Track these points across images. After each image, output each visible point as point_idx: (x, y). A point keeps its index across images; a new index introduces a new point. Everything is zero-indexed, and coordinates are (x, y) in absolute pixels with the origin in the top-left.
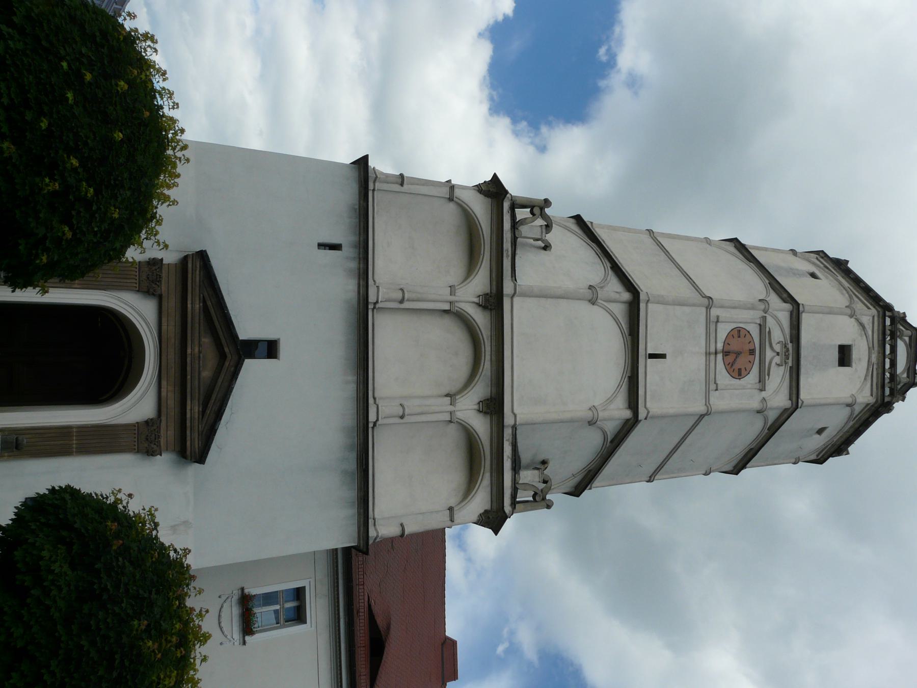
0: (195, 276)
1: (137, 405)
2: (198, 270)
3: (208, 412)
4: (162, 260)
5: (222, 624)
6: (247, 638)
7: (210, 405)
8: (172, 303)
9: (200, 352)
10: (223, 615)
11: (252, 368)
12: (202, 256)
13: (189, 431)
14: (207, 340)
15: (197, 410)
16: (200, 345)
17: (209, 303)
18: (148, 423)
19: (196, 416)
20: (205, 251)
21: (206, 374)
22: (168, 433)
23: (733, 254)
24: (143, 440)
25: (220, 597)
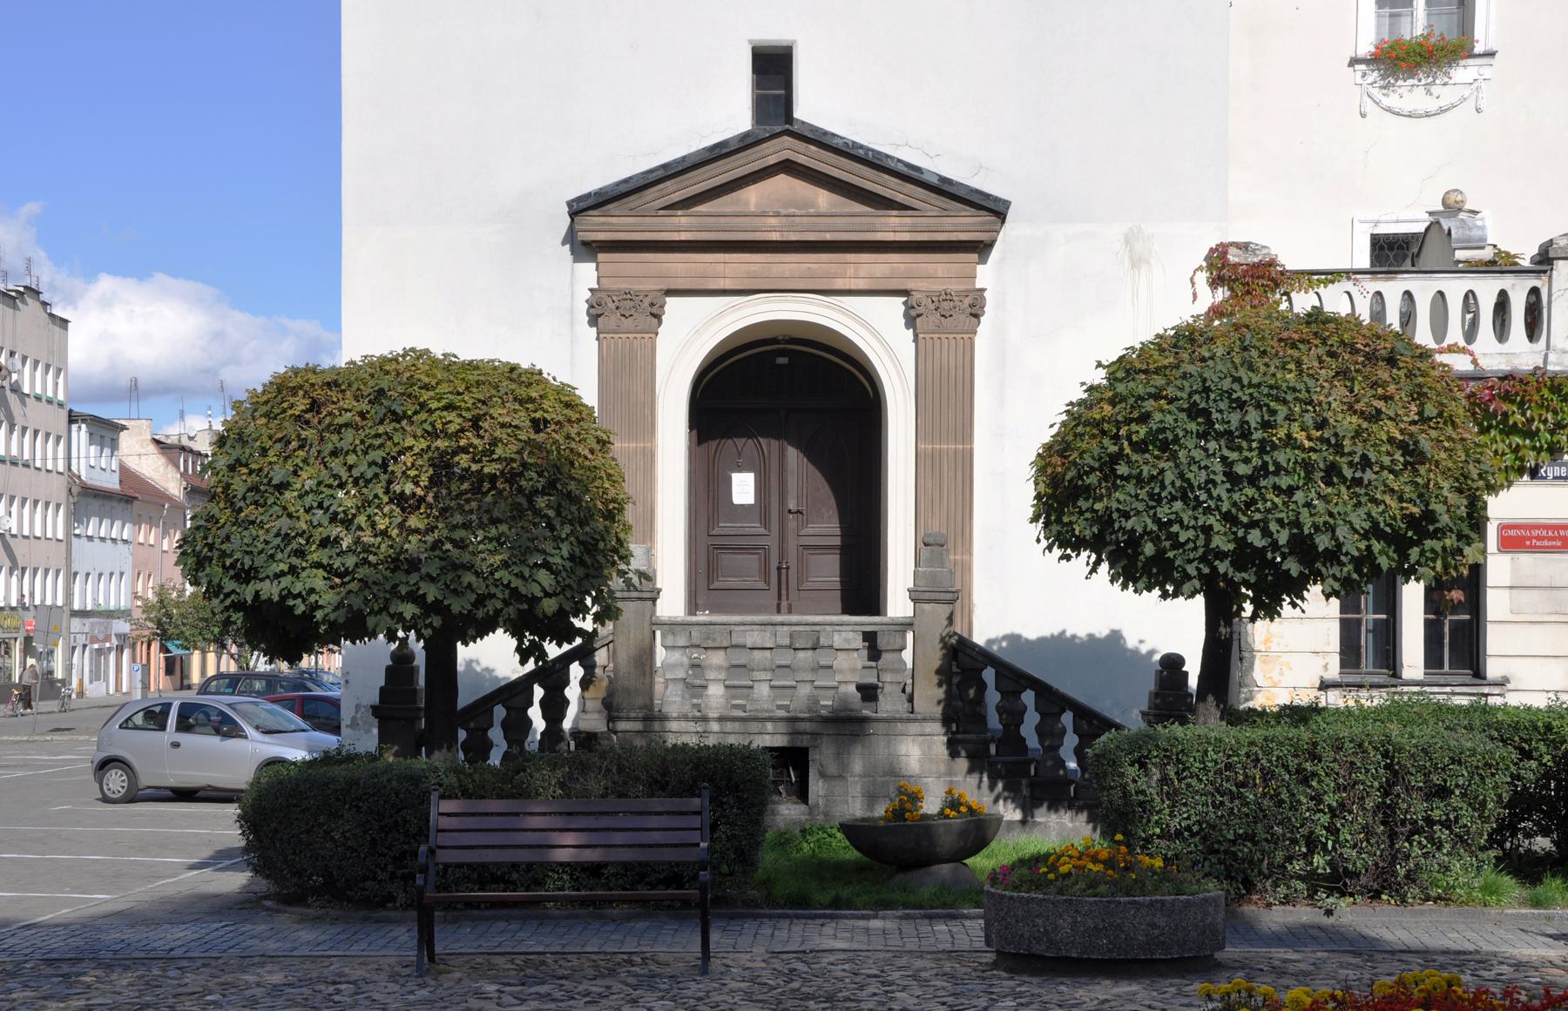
0: (599, 227)
1: (878, 331)
2: (604, 223)
3: (900, 198)
5: (1421, 109)
6: (1479, 49)
7: (887, 193)
9: (777, 215)
10: (1407, 108)
12: (580, 208)
13: (939, 223)
14: (752, 196)
15: (897, 220)
16: (764, 215)
17: (676, 197)
18: (911, 320)
19: (908, 220)
21: (823, 199)
22: (937, 271)
23: (888, 156)
24: (947, 322)
25: (1363, 115)
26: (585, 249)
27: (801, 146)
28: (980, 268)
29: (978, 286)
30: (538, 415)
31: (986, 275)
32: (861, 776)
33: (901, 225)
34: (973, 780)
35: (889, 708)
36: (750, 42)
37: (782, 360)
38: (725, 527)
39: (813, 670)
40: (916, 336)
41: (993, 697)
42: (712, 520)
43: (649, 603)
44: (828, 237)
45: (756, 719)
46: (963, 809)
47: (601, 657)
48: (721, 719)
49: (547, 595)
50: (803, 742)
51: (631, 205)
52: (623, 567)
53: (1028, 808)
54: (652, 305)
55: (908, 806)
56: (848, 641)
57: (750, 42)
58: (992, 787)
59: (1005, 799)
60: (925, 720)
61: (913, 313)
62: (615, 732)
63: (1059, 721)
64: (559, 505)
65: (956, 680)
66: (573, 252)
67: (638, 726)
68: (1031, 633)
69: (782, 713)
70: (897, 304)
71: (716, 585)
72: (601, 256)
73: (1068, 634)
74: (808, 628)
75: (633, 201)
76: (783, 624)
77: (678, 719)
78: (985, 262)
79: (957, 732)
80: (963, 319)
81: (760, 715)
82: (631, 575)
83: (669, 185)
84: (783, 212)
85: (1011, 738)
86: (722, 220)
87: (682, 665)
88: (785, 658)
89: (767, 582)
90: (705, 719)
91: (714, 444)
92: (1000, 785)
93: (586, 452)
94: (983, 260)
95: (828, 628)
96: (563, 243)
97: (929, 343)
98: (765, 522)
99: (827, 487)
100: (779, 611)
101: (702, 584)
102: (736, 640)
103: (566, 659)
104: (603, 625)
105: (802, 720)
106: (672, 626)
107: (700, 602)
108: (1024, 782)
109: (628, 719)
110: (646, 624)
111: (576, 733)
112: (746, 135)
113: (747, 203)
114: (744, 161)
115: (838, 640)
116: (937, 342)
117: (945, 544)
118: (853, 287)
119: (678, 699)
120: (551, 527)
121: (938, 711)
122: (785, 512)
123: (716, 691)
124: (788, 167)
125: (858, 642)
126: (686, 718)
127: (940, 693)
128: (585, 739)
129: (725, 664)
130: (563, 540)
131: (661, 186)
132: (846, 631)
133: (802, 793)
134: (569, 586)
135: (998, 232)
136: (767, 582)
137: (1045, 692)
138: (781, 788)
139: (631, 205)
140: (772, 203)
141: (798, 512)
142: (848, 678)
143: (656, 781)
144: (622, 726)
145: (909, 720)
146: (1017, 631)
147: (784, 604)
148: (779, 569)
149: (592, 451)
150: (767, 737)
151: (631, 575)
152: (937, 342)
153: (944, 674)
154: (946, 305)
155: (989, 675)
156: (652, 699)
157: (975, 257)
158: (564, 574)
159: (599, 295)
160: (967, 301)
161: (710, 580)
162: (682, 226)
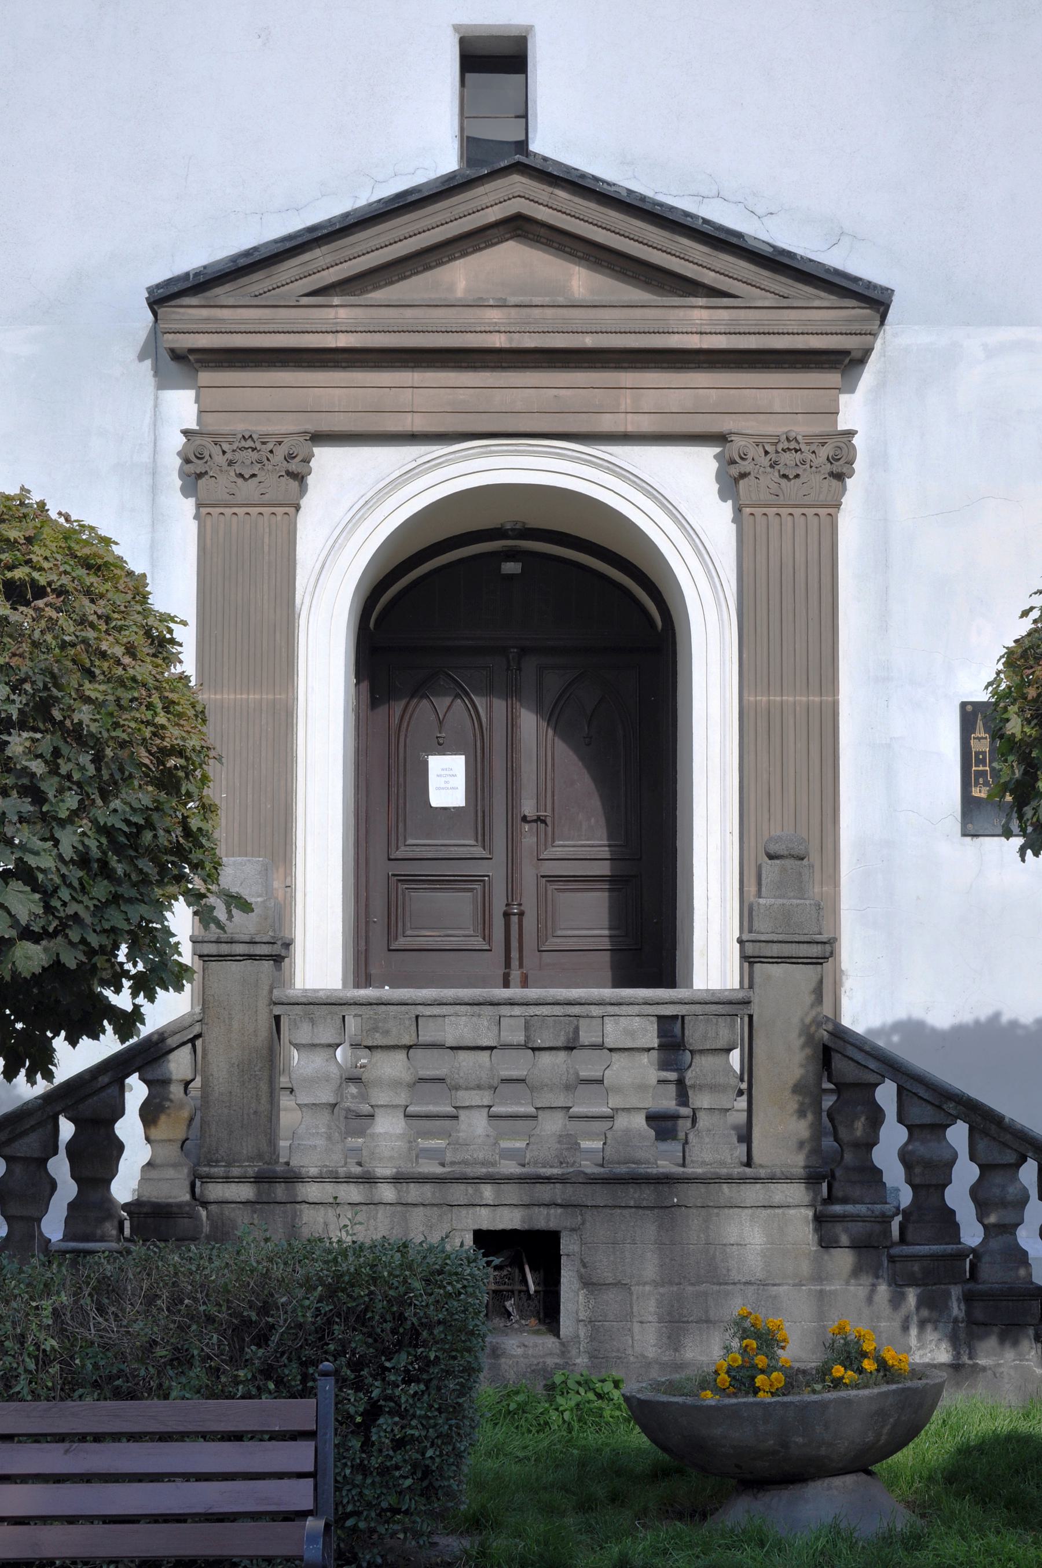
0: (204, 325)
1: (676, 506)
2: (211, 321)
3: (709, 278)
4: (186, 432)
8: (334, 392)
11: (565, 125)
12: (163, 298)
13: (771, 329)
14: (460, 276)
15: (705, 314)
18: (732, 481)
19: (724, 314)
20: (151, 290)
21: (580, 280)
22: (770, 402)
24: (789, 489)
28: (843, 398)
29: (842, 426)
30: (19, 573)
31: (853, 411)
32: (656, 1284)
34: (858, 1290)
35: (708, 1157)
36: (457, 28)
37: (511, 568)
38: (417, 844)
39: (569, 1088)
40: (738, 510)
41: (893, 1135)
42: (395, 834)
43: (268, 965)
44: (589, 342)
45: (463, 1179)
46: (869, 1365)
47: (179, 1064)
48: (398, 1180)
49: (27, 934)
50: (544, 1220)
51: (256, 288)
52: (197, 883)
53: (965, 1336)
54: (290, 457)
55: (761, 1361)
56: (631, 1033)
57: (457, 28)
58: (897, 1301)
59: (922, 1324)
60: (772, 1179)
61: (734, 471)
62: (205, 1204)
63: (1015, 1178)
64: (56, 753)
65: (828, 1102)
66: (157, 371)
67: (245, 1192)
68: (941, 1018)
69: (510, 1168)
71: (401, 942)
72: (205, 377)
73: (1005, 1019)
74: (558, 1010)
75: (258, 282)
76: (512, 1003)
77: (319, 1179)
78: (852, 390)
79: (830, 1199)
80: (816, 483)
81: (469, 1171)
82: (212, 900)
83: (318, 256)
84: (513, 300)
85: (932, 1213)
86: (409, 313)
87: (328, 1079)
88: (516, 1065)
89: (487, 937)
90: (368, 1180)
91: (398, 707)
92: (912, 1297)
93: (119, 651)
95: (595, 1011)
96: (142, 357)
98: (484, 837)
99: (587, 779)
100: (506, 985)
101: (378, 931)
102: (425, 1037)
103: (114, 1071)
104: (151, 998)
105: (548, 1180)
106: (317, 1005)
107: (373, 971)
108: (956, 1291)
109: (227, 1179)
110: (262, 1004)
111: (134, 1208)
112: (452, 176)
113: (451, 288)
114: (446, 216)
115: (614, 1033)
116: (774, 521)
117: (793, 858)
118: (630, 429)
119: (320, 1142)
120: (38, 797)
121: (797, 1161)
122: (516, 819)
123: (389, 1127)
124: (519, 227)
125: (651, 1037)
126: (335, 1178)
127: (801, 1128)
128: (151, 1218)
129: (407, 1077)
130: (62, 823)
131: (307, 257)
132: (629, 1018)
133: (548, 1312)
134: (76, 916)
135: (874, 335)
136: (487, 937)
137: (985, 1123)
138: (509, 1304)
139: (256, 288)
140: (494, 287)
141: (539, 820)
142: (633, 1102)
143: (248, 1323)
144: (216, 1191)
145: (743, 1180)
146: (918, 1014)
147: (515, 974)
148: (507, 915)
149: (131, 650)
150: (484, 1212)
151: (212, 900)
152: (774, 521)
153: (808, 1095)
154: (788, 458)
155: (886, 1094)
156: (272, 1142)
157: (833, 378)
158: (65, 894)
159: (198, 441)
160: (824, 452)
161: (391, 931)
162: (342, 323)
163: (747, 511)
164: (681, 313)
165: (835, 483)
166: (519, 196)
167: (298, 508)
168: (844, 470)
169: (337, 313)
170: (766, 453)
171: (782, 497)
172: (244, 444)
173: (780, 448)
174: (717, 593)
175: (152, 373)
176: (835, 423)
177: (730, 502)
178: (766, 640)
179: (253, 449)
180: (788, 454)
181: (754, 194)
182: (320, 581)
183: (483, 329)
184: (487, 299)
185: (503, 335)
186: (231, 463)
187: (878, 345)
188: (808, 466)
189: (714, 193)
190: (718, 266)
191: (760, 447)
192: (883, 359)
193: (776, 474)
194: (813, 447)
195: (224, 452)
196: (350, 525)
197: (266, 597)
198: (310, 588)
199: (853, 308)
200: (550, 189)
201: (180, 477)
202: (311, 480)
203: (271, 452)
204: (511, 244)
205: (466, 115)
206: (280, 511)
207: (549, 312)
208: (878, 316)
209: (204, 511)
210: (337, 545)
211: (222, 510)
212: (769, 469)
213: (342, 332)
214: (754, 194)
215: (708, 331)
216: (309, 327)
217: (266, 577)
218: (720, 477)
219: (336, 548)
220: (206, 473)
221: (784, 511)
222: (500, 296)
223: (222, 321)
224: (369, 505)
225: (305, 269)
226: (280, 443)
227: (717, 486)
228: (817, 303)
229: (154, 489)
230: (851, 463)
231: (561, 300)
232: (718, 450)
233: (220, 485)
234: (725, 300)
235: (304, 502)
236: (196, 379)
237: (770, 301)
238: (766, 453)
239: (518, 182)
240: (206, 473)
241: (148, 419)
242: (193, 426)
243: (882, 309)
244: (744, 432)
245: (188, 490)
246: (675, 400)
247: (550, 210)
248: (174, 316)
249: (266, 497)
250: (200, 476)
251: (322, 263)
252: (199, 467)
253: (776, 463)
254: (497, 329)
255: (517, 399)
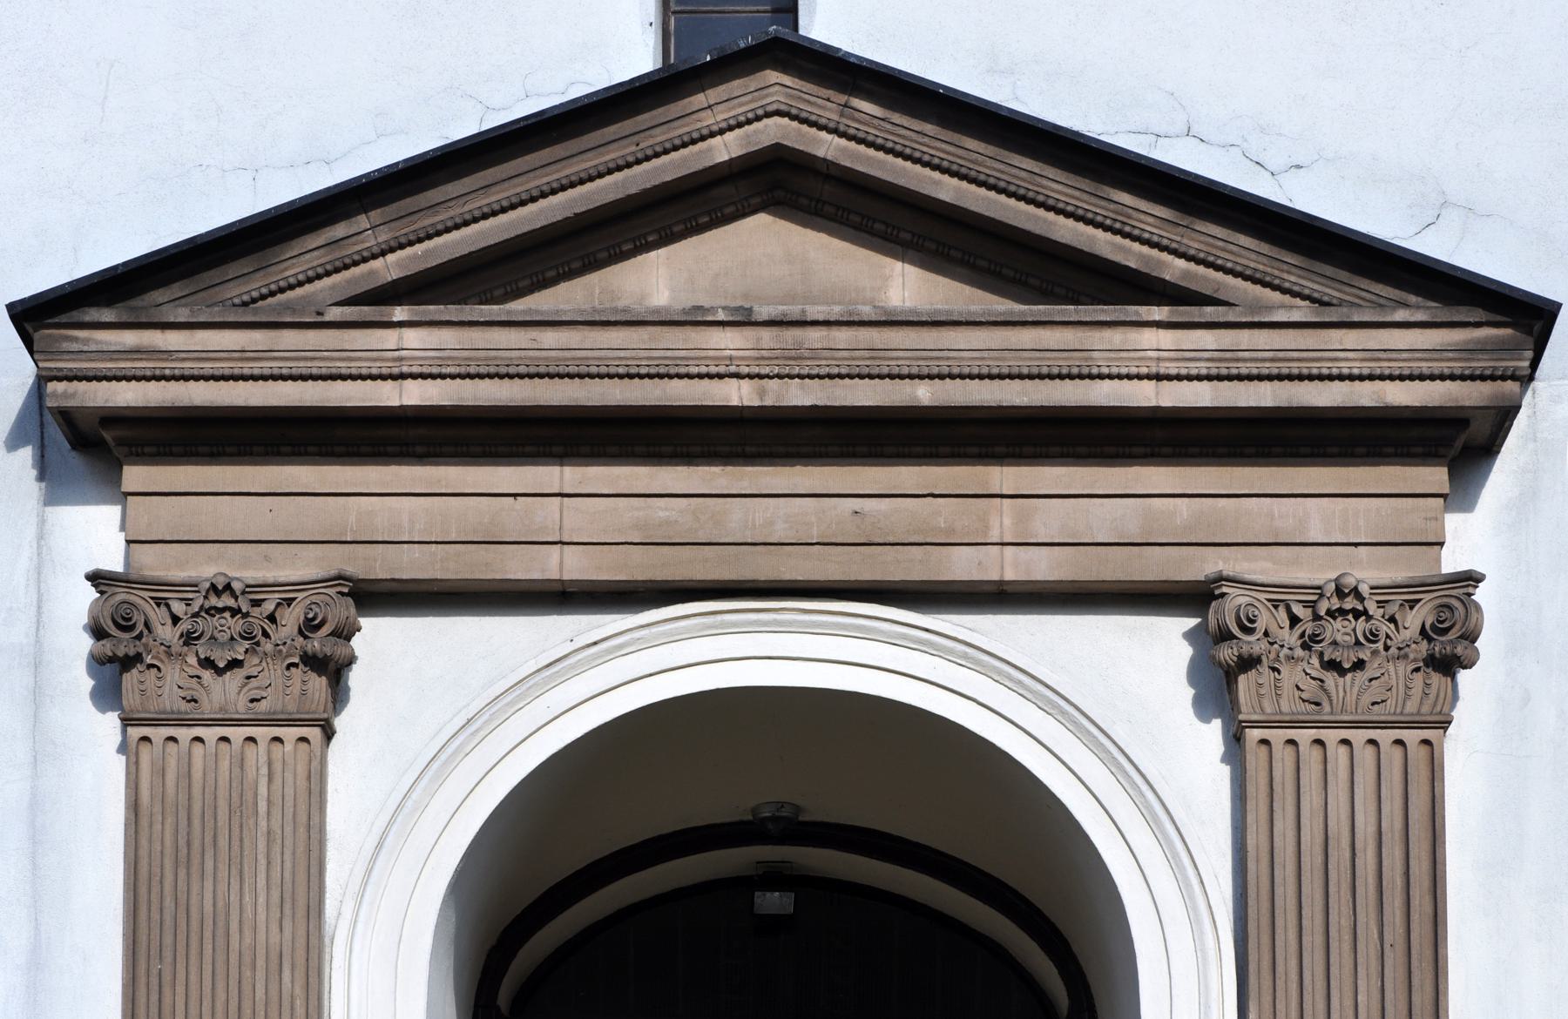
1: (1111, 734)
3: (1174, 269)
9: (743, 320)
14: (656, 277)
15: (1166, 338)
18: (1219, 681)
21: (904, 284)
22: (1307, 528)
26: (87, 446)
27: (823, 102)
28: (1454, 523)
29: (1451, 561)
33: (1181, 354)
37: (773, 902)
40: (1235, 740)
54: (310, 626)
61: (1227, 653)
70: (1165, 642)
72: (135, 476)
80: (1396, 682)
94: (1462, 493)
97: (1284, 756)
114: (628, 150)
116: (1311, 756)
124: (778, 183)
139: (236, 291)
152: (1311, 756)
154: (1338, 630)
157: (1435, 477)
160: (1413, 621)
162: (418, 361)
163: (1254, 734)
164: (1116, 337)
165: (1436, 679)
166: (779, 113)
167: (329, 734)
168: (1459, 650)
169: (400, 338)
170: (1294, 620)
171: (1326, 707)
172: (213, 601)
173: (1322, 608)
174: (1192, 897)
175: (34, 473)
176: (1438, 560)
177: (1217, 724)
178: (1294, 986)
179: (235, 612)
180: (1338, 623)
181: (1262, 130)
182: (375, 873)
183: (704, 370)
184: (712, 310)
185: (745, 383)
186: (189, 639)
187: (1527, 400)
188: (1380, 646)
189: (1181, 127)
190: (1193, 245)
191: (1282, 609)
192: (1531, 446)
193: (1315, 661)
194: (1392, 609)
195: (176, 620)
196: (435, 765)
197: (262, 900)
198: (355, 886)
199: (1478, 325)
200: (843, 98)
201: (92, 672)
202: (356, 678)
203: (272, 618)
204: (762, 219)
205: (673, 7)
206: (290, 733)
207: (842, 336)
208: (1530, 342)
209: (135, 733)
210: (409, 803)
211: (171, 731)
212: (1299, 652)
213: (414, 376)
214: (1262, 130)
215: (1173, 372)
216: (343, 367)
217: (262, 861)
218: (1196, 673)
219: (405, 810)
220: (138, 658)
221: (1331, 736)
222: (739, 303)
223: (167, 354)
224: (473, 728)
225: (338, 255)
226: (290, 601)
227: (1191, 692)
228: (1400, 315)
229: (38, 696)
230: (1471, 637)
231: (867, 312)
232: (1192, 622)
233: (168, 684)
234: (1209, 309)
235: (339, 723)
236: (117, 479)
237: (1301, 311)
238: (1294, 620)
239: (775, 84)
240: (138, 658)
241: (25, 561)
242: (115, 564)
243: (1537, 327)
244: (1248, 577)
245: (107, 695)
246: (1103, 519)
247: (843, 142)
248: (66, 346)
249: (263, 706)
250: (128, 663)
251: (370, 242)
252: (124, 645)
253: (1315, 638)
254: (733, 369)
255: (777, 518)
